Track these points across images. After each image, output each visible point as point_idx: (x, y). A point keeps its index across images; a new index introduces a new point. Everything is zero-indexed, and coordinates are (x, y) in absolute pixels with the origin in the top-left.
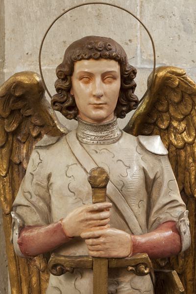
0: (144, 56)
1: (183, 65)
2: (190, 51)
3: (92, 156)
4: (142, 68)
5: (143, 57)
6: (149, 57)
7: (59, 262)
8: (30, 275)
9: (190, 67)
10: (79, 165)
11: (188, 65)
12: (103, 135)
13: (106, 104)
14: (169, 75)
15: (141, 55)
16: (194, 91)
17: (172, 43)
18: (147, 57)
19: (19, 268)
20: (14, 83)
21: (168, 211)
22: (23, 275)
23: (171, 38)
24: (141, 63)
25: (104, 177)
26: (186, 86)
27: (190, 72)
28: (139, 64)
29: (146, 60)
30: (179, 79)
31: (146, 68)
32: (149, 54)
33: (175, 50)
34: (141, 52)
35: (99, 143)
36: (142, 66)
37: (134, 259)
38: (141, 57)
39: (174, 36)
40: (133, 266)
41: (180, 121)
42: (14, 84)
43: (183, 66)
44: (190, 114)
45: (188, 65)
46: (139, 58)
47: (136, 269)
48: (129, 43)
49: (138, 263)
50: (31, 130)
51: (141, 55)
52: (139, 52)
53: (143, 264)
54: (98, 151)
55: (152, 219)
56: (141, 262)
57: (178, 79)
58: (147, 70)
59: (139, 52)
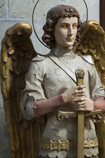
0: (11, 14)
1: (36, 18)
2: (42, 9)
3: (66, 65)
4: (9, 21)
5: (10, 14)
6: (13, 14)
7: (63, 114)
8: (20, 132)
9: (41, 19)
10: (61, 69)
11: (40, 18)
12: (68, 55)
13: (73, 39)
14: (93, 25)
15: (9, 13)
16: (103, 33)
17: (28, 5)
18: (12, 14)
19: (14, 129)
20: (19, 28)
21: (100, 92)
22: (17, 132)
23: (28, 3)
24: (9, 18)
25: (82, 73)
26: (100, 30)
27: (41, 22)
28: (8, 18)
29: (11, 16)
30: (97, 27)
31: (12, 21)
32: (14, 12)
33: (30, 9)
34: (8, 11)
35: (70, 58)
36: (9, 19)
37: (95, 112)
38: (9, 14)
39: (30, 1)
40: (95, 115)
41: (93, 49)
42: (19, 29)
43: (36, 18)
44: (99, 45)
45: (40, 18)
46: (7, 15)
47: (96, 117)
48: (2, 6)
49: (97, 114)
50: (20, 53)
51: (9, 13)
52: (7, 11)
53: (99, 114)
54: (68, 63)
55: (93, 95)
56: (98, 113)
57: (96, 27)
58: (12, 21)
59: (7, 11)
